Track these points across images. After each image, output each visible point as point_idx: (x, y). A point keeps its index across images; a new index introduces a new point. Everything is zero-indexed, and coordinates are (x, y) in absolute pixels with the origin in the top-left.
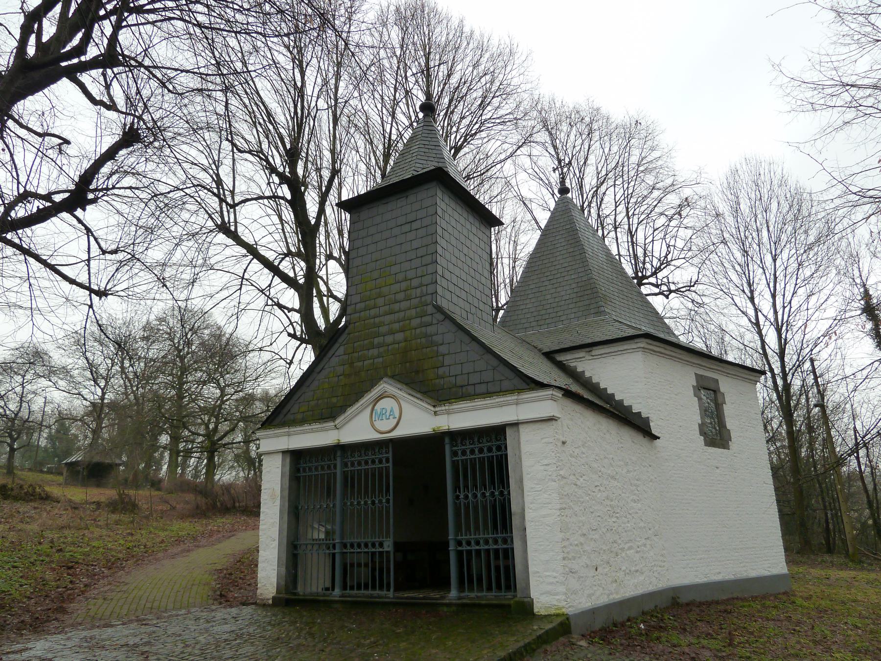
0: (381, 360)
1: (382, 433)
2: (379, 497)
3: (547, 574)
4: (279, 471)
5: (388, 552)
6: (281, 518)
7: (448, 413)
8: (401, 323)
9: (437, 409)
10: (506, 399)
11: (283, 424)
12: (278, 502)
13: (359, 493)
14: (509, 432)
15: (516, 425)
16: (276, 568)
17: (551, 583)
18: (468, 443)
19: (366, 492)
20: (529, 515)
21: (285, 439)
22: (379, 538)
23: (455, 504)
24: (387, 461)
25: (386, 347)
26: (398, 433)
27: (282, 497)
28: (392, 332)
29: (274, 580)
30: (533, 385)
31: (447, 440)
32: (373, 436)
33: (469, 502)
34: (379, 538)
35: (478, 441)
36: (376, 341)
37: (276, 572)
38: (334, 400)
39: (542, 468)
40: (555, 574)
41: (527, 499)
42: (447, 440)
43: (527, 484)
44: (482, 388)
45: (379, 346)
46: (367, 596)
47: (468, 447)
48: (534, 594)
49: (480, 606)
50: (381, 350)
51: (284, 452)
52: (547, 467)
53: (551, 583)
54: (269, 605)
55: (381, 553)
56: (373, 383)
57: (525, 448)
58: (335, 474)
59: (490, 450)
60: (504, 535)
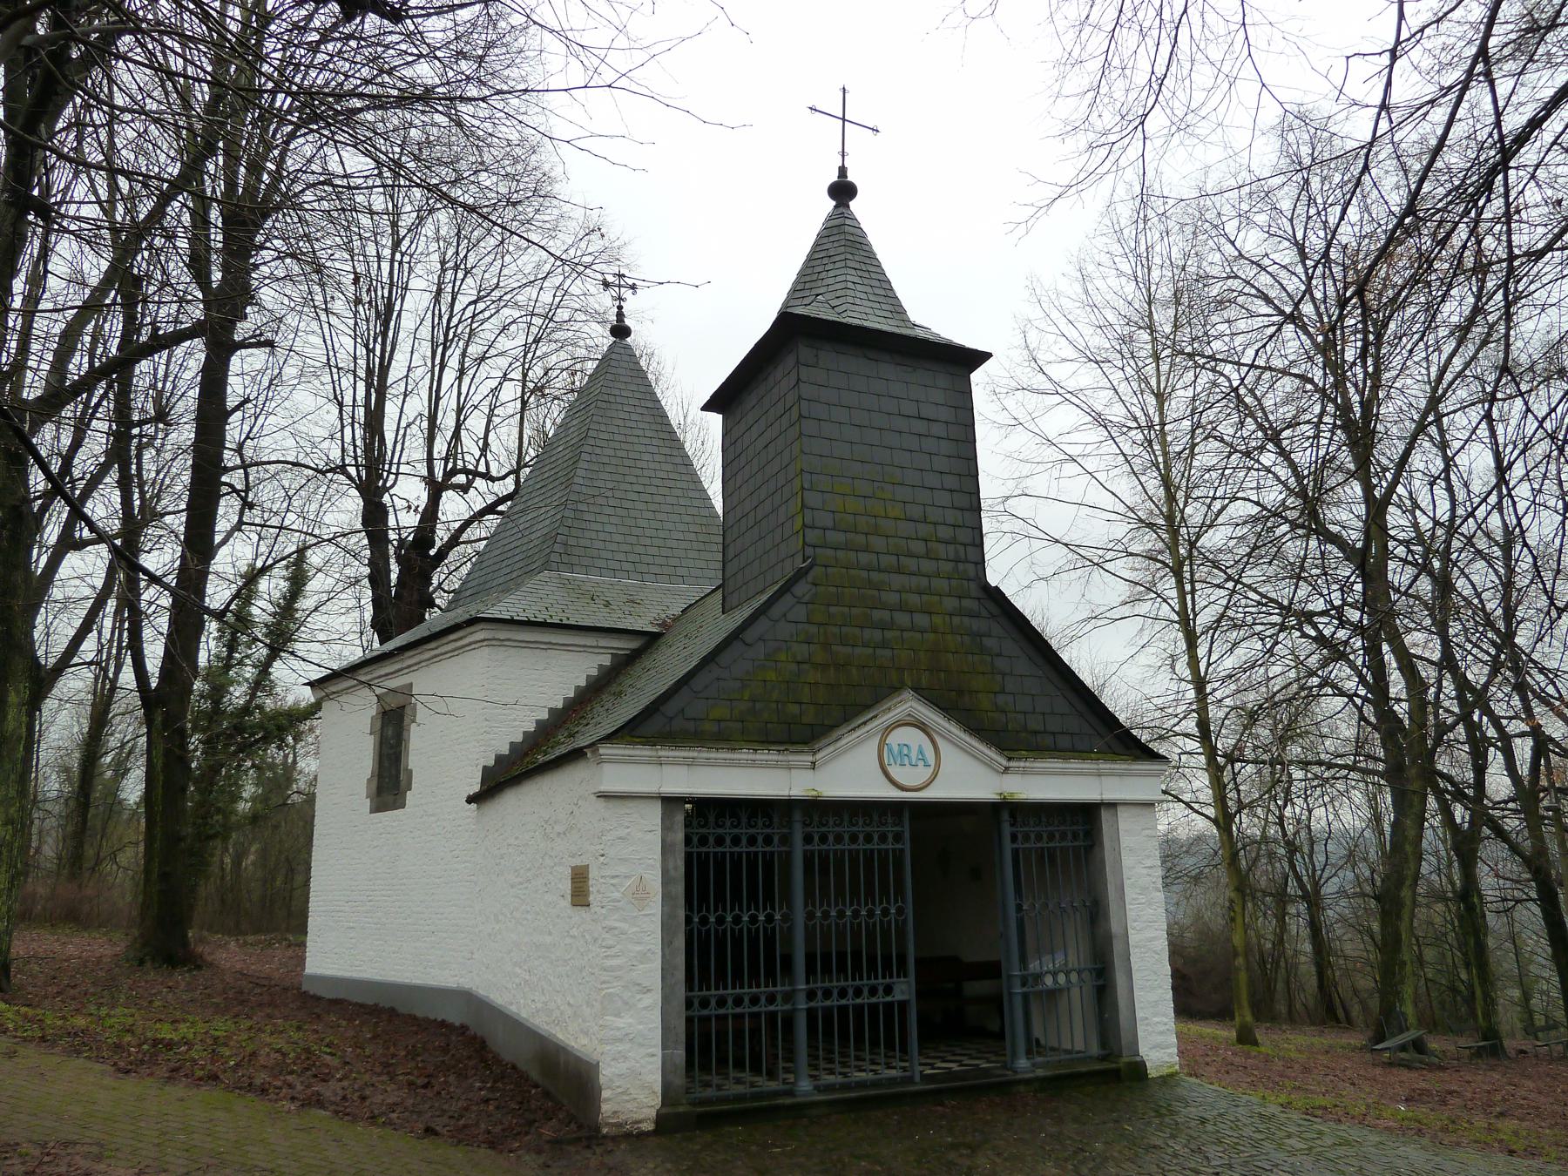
0: (888, 653)
1: (903, 789)
2: (866, 904)
3: (1156, 1019)
4: (656, 839)
5: (903, 1005)
6: (666, 942)
7: (1025, 772)
8: (925, 598)
9: (1012, 764)
10: (1113, 766)
11: (651, 741)
12: (655, 908)
13: (840, 892)
14: (1105, 815)
15: (1113, 805)
16: (659, 1051)
17: (1161, 1033)
18: (831, 823)
19: (720, 898)
20: (1133, 938)
21: (780, 774)
22: (884, 977)
23: (790, 906)
24: (898, 837)
25: (898, 633)
26: (935, 793)
27: (666, 897)
28: (902, 607)
29: (655, 1079)
30: (1139, 752)
31: (1005, 816)
32: (882, 791)
33: (725, 929)
34: (839, 980)
35: (851, 821)
36: (877, 615)
37: (657, 1062)
38: (794, 709)
39: (1145, 871)
40: (1165, 1020)
41: (1131, 914)
42: (1005, 816)
43: (1130, 893)
44: (1064, 741)
45: (883, 627)
46: (875, 1084)
47: (728, 831)
48: (1144, 1050)
49: (1080, 1075)
50: (889, 634)
51: (670, 802)
52: (1150, 871)
53: (1161, 1033)
54: (642, 1135)
55: (889, 1006)
56: (895, 689)
57: (1126, 841)
58: (789, 854)
59: (752, 841)
60: (754, 990)
